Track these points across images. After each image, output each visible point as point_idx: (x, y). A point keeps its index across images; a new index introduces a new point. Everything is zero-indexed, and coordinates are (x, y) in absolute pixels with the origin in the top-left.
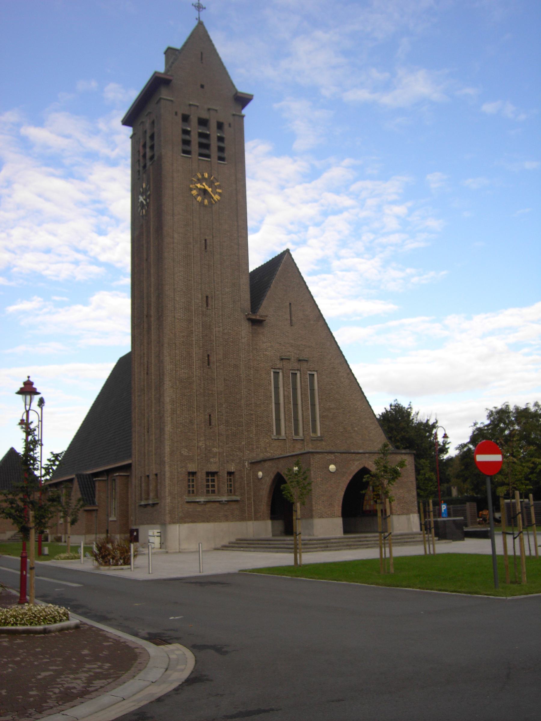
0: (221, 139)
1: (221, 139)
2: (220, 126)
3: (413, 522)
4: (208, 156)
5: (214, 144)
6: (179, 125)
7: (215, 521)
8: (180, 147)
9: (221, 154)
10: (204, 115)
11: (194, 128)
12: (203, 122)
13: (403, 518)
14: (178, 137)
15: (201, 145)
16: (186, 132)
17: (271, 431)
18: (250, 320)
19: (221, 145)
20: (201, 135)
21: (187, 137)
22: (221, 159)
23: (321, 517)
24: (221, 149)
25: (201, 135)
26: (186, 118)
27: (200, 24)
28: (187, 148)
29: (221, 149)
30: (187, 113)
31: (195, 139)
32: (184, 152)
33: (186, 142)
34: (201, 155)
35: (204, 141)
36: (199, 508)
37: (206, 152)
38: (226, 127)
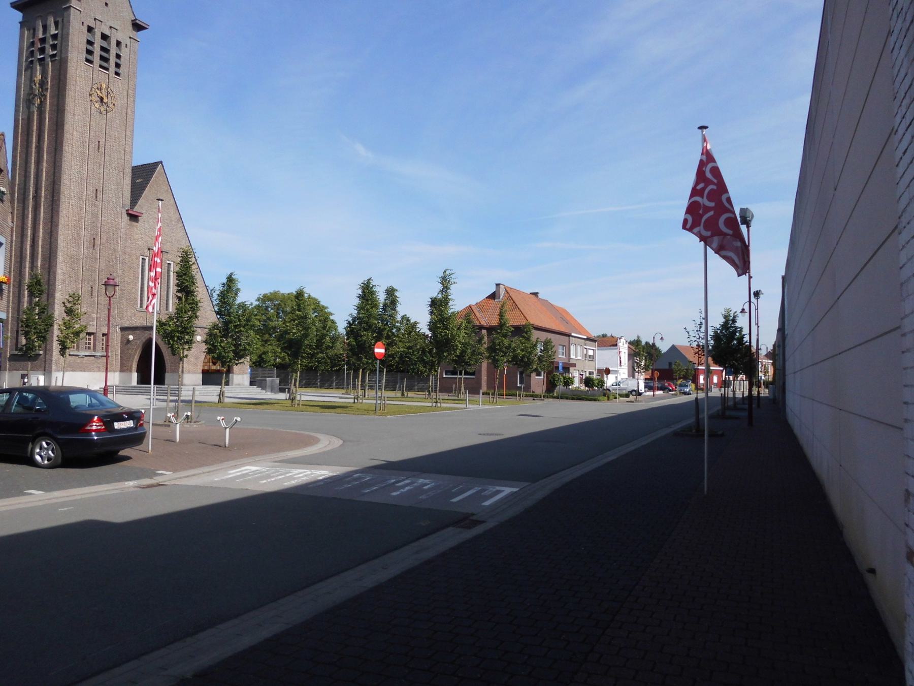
0: (118, 56)
1: (118, 56)
2: (118, 43)
3: (246, 379)
4: (107, 69)
5: (113, 59)
6: (85, 36)
7: (89, 370)
8: (84, 55)
9: (117, 70)
10: (107, 32)
11: (98, 42)
12: (104, 37)
13: (240, 376)
14: (84, 46)
15: (102, 58)
16: (90, 43)
17: (136, 304)
18: (129, 214)
19: (118, 61)
20: (102, 49)
21: (90, 48)
22: (117, 74)
23: (189, 373)
24: (118, 65)
25: (102, 49)
26: (90, 29)
27: (708, 158)
28: (89, 57)
29: (118, 65)
30: (92, 25)
31: (97, 52)
32: (87, 60)
33: (89, 52)
34: (101, 66)
35: (104, 54)
36: (78, 360)
37: (105, 64)
38: (123, 46)
